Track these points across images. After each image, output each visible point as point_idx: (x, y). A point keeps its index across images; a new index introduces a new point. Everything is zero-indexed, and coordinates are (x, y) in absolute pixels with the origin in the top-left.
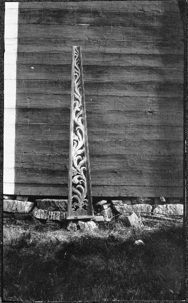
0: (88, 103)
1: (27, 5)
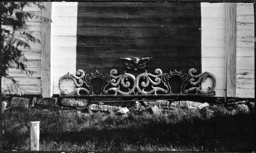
0: (105, 107)
1: (83, 4)
